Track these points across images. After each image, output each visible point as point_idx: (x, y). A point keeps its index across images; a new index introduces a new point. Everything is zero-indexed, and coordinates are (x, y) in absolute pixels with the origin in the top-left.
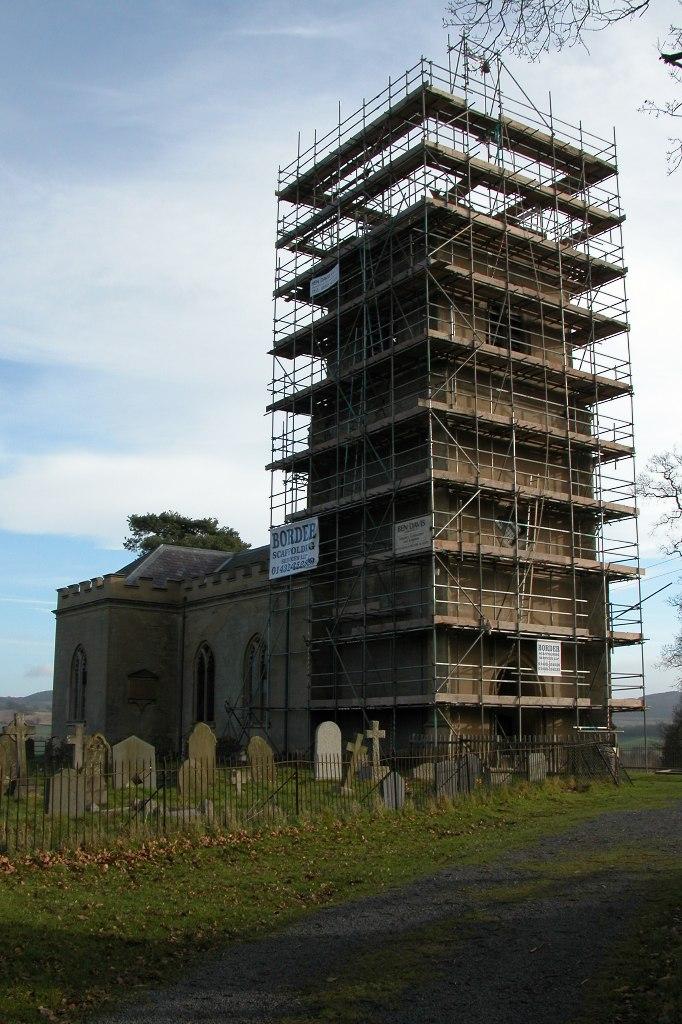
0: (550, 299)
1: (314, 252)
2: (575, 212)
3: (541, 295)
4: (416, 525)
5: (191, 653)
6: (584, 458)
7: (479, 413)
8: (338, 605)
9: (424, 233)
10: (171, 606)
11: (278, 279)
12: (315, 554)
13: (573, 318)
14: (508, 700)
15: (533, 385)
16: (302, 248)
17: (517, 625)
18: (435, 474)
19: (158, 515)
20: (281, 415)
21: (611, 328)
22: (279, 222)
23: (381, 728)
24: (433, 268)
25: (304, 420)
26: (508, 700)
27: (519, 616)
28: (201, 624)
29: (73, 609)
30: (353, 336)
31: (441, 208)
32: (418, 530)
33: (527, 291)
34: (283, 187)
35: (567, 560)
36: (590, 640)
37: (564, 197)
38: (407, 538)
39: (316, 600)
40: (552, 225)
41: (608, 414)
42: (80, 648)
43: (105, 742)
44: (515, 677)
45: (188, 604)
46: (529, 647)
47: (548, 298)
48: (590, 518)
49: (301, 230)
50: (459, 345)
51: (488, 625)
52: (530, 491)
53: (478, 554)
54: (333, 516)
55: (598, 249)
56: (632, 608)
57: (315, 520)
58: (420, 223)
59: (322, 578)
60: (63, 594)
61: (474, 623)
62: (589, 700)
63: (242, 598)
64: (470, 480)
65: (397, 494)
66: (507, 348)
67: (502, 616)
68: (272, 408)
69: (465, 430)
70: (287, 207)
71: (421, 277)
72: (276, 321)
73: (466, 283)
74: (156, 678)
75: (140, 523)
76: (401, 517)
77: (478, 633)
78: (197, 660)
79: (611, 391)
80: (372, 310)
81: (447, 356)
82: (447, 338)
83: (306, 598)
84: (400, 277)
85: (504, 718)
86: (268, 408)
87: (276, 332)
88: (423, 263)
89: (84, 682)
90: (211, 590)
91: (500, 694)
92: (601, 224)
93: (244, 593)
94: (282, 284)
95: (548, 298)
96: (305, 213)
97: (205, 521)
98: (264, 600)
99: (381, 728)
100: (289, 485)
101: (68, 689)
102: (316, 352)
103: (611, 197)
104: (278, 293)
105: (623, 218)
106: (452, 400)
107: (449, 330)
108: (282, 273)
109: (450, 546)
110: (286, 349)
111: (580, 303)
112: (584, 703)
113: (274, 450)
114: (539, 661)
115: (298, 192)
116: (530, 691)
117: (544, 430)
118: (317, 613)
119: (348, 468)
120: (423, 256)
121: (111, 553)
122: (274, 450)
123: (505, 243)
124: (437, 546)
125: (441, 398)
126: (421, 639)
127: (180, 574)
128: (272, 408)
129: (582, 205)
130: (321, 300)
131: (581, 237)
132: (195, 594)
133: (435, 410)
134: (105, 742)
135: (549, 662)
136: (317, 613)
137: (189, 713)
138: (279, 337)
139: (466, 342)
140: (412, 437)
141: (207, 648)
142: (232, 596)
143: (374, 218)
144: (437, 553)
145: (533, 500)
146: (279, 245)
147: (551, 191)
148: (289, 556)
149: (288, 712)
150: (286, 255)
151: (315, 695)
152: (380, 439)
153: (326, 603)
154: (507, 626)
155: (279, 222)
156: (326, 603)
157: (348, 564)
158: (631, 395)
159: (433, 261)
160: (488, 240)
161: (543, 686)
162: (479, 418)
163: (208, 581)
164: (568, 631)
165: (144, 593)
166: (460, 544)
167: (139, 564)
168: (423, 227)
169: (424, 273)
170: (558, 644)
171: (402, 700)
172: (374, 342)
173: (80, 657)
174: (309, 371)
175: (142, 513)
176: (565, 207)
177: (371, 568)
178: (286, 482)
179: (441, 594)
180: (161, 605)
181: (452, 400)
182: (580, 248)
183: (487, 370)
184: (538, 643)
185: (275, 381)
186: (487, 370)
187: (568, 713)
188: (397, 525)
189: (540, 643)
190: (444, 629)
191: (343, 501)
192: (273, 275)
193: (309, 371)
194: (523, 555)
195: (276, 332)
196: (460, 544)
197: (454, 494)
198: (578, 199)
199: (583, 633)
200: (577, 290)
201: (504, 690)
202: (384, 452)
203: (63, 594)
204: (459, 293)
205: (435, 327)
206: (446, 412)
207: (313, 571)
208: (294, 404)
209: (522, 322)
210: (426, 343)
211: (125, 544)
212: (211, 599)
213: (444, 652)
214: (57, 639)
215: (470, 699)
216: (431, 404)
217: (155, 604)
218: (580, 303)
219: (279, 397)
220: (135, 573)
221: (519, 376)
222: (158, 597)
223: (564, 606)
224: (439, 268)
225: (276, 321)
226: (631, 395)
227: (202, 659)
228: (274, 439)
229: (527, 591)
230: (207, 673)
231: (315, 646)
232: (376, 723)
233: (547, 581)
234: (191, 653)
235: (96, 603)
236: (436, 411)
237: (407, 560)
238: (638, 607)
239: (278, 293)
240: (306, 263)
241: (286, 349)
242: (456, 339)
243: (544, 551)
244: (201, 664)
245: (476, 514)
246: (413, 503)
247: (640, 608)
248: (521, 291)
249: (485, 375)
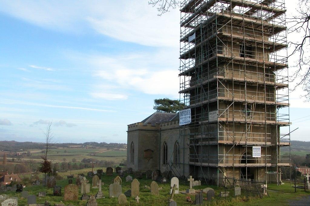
0: (258, 40)
1: (192, 27)
2: (270, 11)
3: (256, 39)
4: (214, 113)
5: (162, 144)
6: (271, 89)
7: (234, 78)
8: (196, 135)
9: (216, 24)
10: (157, 131)
11: (181, 36)
12: (190, 119)
13: (267, 45)
14: (243, 165)
15: (252, 67)
16: (188, 26)
17: (246, 142)
18: (219, 98)
19: (163, 99)
20: (183, 77)
21: (279, 47)
22: (181, 19)
23: (192, 178)
24: (218, 35)
25: (188, 78)
26: (243, 165)
27: (246, 140)
28: (165, 137)
29: (131, 131)
30: (199, 55)
31: (221, 16)
32: (215, 115)
33: (251, 38)
34: (182, 8)
35: (264, 121)
36: (271, 145)
37: (265, 6)
38: (213, 116)
39: (191, 133)
40: (260, 14)
41: (280, 75)
42: (132, 142)
43: (120, 178)
44: (245, 158)
45: (161, 130)
46: (250, 148)
47: (258, 40)
48: (272, 108)
49: (187, 21)
50: (227, 58)
51: (236, 143)
52: (250, 101)
53: (265, 103)
54: (194, 108)
55: (277, 22)
56: (287, 135)
57: (190, 109)
58: (214, 22)
59: (193, 126)
60: (129, 126)
61: (232, 142)
62: (271, 164)
63: (174, 130)
64: (231, 99)
65: (209, 103)
66: (244, 57)
67: (242, 139)
68: (180, 75)
69: (229, 83)
70: (183, 14)
71: (215, 37)
72: (181, 49)
73: (230, 38)
74: (153, 151)
75: (157, 102)
76: (211, 110)
77: (233, 145)
78: (164, 147)
79: (281, 67)
80: (204, 46)
81: (224, 62)
82: (223, 56)
83: (188, 132)
84: (210, 37)
85: (243, 169)
86: (179, 75)
87: (181, 52)
88: (216, 33)
89: (134, 152)
90: (167, 127)
91: (241, 163)
92: (278, 13)
93: (174, 129)
94: (182, 37)
95: (258, 40)
96: (189, 15)
97: (176, 101)
98: (178, 131)
99: (192, 178)
100: (186, 98)
101: (130, 154)
102: (193, 57)
103: (282, 4)
104: (181, 41)
105: (286, 11)
106: (228, 74)
107: (227, 53)
108: (182, 34)
109: (224, 120)
110: (184, 57)
111: (271, 40)
112: (269, 165)
113: (180, 87)
114: (253, 153)
115: (186, 10)
116: (249, 162)
117: (256, 82)
118: (191, 136)
119: (198, 94)
120: (215, 32)
121: (145, 111)
122: (180, 87)
123: (243, 24)
124: (220, 120)
125: (223, 74)
126: (215, 146)
127: (160, 121)
128: (180, 75)
129: (271, 8)
130: (193, 42)
131: (270, 19)
132: (163, 128)
133: (219, 79)
134: (120, 178)
135: (257, 153)
136: (191, 136)
137: (162, 163)
138: (182, 54)
139: (230, 57)
140: (213, 86)
141: (166, 143)
142: (171, 129)
143: (211, 14)
144: (220, 122)
145: (252, 104)
146: (181, 26)
147: (260, 5)
148: (184, 119)
149: (184, 164)
150: (183, 28)
151: (191, 160)
152: (205, 86)
153: (193, 134)
154: (243, 142)
155: (181, 19)
156: (193, 134)
157: (198, 123)
158: (288, 67)
159: (218, 33)
160: (238, 24)
161: (257, 160)
162: (234, 80)
163: (166, 124)
164: (264, 143)
165: (149, 127)
166: (227, 119)
167: (147, 119)
168: (215, 23)
169: (215, 37)
170: (260, 147)
171: (211, 165)
172: (206, 57)
173: (133, 145)
174: (191, 63)
175: (158, 99)
176: (265, 9)
177: (205, 124)
178: (184, 97)
179: (221, 134)
180: (154, 131)
181: (228, 74)
182: (271, 23)
183: (239, 63)
184: (253, 147)
185: (181, 67)
186: (239, 63)
187: (264, 168)
188: (209, 113)
189: (253, 147)
190: (221, 145)
191: (197, 104)
192: (180, 35)
193: (191, 63)
194: (248, 121)
195: (181, 52)
196: (227, 119)
197: (227, 103)
198: (270, 6)
199: (269, 144)
200: (269, 36)
201: (243, 162)
202: (206, 90)
203: (129, 126)
204: (227, 41)
205: (219, 53)
206: (223, 79)
207: (189, 124)
208: (185, 74)
209: (250, 49)
210: (216, 58)
211: (154, 108)
212: (166, 130)
213: (222, 152)
214: (128, 141)
215: (230, 165)
216: (218, 77)
217: (152, 130)
218: (271, 40)
219: (182, 72)
220: (147, 121)
221: (250, 64)
222: (153, 128)
223: (264, 135)
224: (220, 35)
225: (181, 49)
226: (288, 67)
227: (165, 146)
228: (180, 84)
229: (250, 132)
230: (166, 150)
231: (191, 146)
232: (191, 177)
233: (256, 128)
234: (162, 144)
235: (136, 130)
236: (220, 79)
237: (213, 123)
238: (289, 134)
239: (181, 41)
240: (188, 31)
241: (184, 57)
242: (226, 56)
243: (259, 119)
244: (164, 147)
245: (233, 109)
246: (213, 106)
247: (289, 135)
248: (248, 38)
249: (237, 65)
